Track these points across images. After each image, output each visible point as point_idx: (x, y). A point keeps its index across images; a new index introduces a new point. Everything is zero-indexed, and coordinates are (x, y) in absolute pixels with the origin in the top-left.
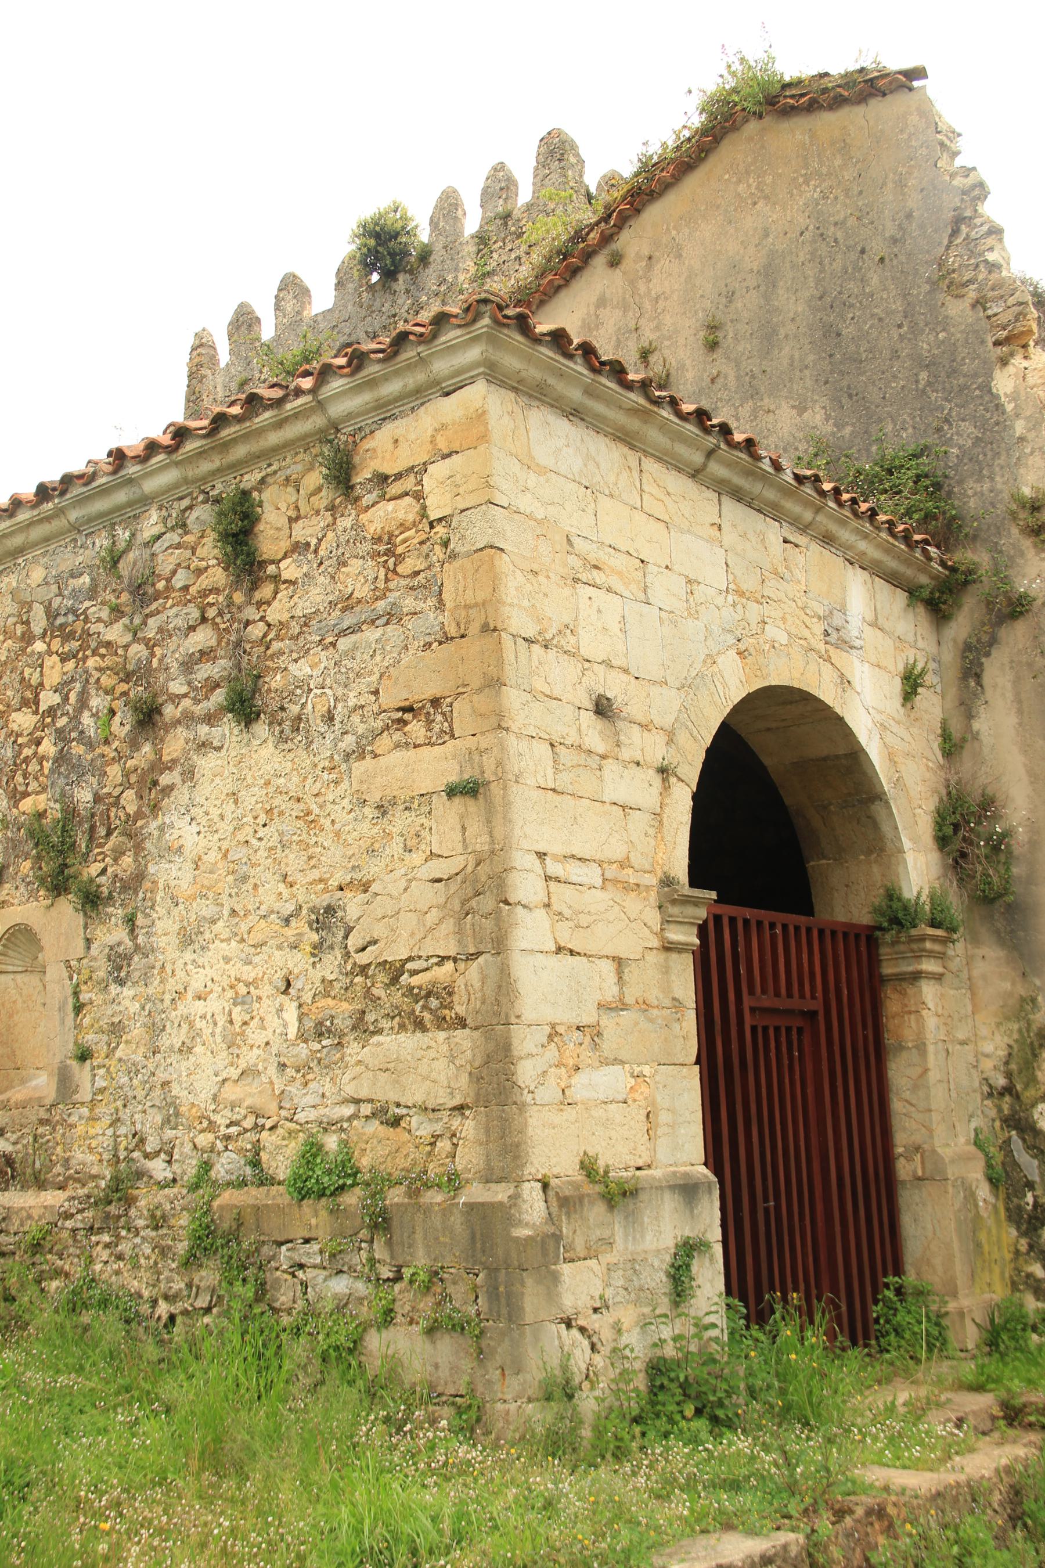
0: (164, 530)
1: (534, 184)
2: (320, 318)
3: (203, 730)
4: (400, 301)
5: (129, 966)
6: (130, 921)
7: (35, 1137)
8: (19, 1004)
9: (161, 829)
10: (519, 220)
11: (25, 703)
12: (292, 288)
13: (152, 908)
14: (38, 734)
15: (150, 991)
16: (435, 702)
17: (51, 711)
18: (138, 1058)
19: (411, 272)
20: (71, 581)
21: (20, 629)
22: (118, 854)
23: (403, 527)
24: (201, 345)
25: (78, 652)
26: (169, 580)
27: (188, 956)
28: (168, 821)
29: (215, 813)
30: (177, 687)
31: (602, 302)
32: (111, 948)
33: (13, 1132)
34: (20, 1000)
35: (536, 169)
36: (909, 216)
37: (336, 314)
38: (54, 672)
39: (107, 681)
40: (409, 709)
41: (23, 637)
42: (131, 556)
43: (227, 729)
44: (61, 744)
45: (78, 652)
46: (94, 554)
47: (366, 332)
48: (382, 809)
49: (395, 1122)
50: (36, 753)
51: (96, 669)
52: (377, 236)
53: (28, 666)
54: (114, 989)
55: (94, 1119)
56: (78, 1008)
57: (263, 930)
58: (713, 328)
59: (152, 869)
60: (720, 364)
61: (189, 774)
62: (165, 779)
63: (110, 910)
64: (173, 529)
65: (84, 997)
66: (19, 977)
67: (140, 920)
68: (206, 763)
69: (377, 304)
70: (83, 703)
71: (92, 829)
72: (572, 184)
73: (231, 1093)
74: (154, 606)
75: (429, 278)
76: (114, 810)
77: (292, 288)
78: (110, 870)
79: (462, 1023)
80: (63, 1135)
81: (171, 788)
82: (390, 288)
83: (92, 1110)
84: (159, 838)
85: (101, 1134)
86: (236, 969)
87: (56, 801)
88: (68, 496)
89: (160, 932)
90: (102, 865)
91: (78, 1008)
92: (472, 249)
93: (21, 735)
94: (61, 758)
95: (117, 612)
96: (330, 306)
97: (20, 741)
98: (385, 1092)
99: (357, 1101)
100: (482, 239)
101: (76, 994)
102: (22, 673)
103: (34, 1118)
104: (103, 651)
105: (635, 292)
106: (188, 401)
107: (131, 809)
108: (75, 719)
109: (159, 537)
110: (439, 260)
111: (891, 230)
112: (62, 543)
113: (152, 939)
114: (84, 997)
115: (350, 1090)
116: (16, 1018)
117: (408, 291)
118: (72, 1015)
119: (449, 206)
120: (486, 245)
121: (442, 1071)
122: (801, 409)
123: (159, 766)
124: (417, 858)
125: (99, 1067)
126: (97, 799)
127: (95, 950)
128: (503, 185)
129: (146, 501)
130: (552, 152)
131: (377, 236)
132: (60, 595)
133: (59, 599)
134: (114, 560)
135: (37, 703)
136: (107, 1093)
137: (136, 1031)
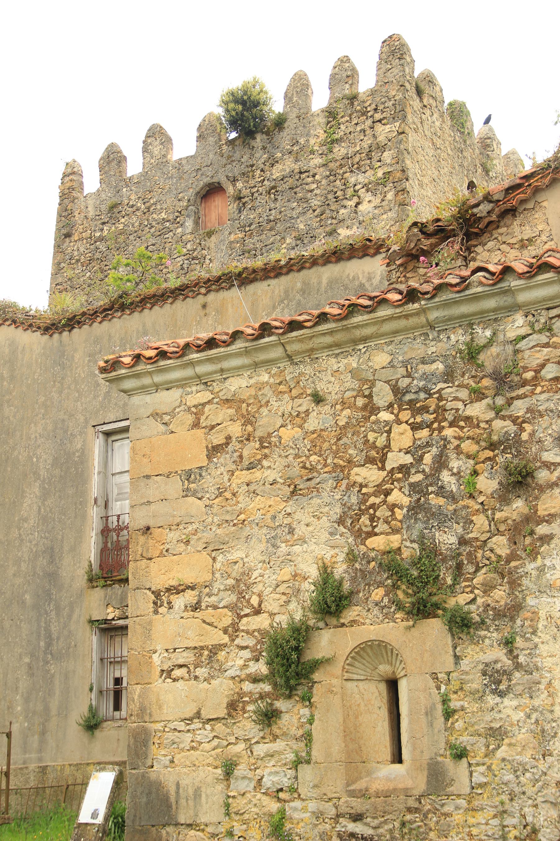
0: (530, 332)
1: (377, 75)
2: (184, 162)
4: (257, 155)
5: (510, 680)
6: (508, 643)
7: (403, 824)
8: (362, 707)
9: (541, 570)
10: (364, 102)
11: (370, 461)
12: (157, 136)
13: (534, 633)
14: (388, 486)
15: (536, 702)
17: (404, 469)
18: (526, 758)
19: (267, 133)
20: (420, 366)
21: (360, 402)
22: (488, 588)
24: (73, 173)
25: (432, 423)
26: (537, 371)
28: (548, 562)
32: (487, 665)
33: (374, 818)
34: (362, 704)
35: (379, 64)
37: (199, 160)
38: (402, 437)
39: (468, 446)
41: (364, 408)
42: (494, 350)
44: (416, 497)
45: (432, 423)
46: (447, 346)
47: (227, 177)
50: (385, 502)
51: (455, 438)
52: (244, 103)
53: (374, 431)
55: (473, 810)
56: (448, 714)
59: (531, 601)
62: (542, 530)
63: (483, 633)
64: (540, 331)
65: (455, 704)
66: (361, 684)
67: (519, 642)
69: (237, 155)
70: (441, 463)
71: (459, 566)
72: (408, 78)
74: (521, 391)
75: (284, 139)
76: (481, 552)
77: (157, 136)
78: (480, 601)
80: (437, 822)
82: (248, 144)
83: (469, 802)
84: (538, 577)
87: (412, 541)
88: (437, 299)
89: (545, 654)
90: (472, 596)
92: (322, 120)
93: (366, 486)
94: (415, 509)
95: (478, 395)
96: (193, 154)
97: (364, 490)
100: (331, 114)
101: (445, 701)
102: (366, 436)
103: (401, 806)
104: (462, 424)
106: (60, 215)
107: (504, 552)
108: (433, 476)
109: (524, 337)
110: (292, 126)
112: (411, 335)
113: (534, 659)
114: (455, 704)
116: (360, 718)
117: (264, 148)
118: (443, 719)
119: (300, 87)
120: (334, 118)
123: (531, 519)
125: (478, 765)
126: (462, 542)
127: (465, 664)
128: (349, 73)
129: (514, 308)
130: (393, 53)
131: (244, 103)
132: (409, 376)
133: (407, 381)
134: (472, 354)
135: (383, 460)
136: (489, 788)
137: (521, 736)
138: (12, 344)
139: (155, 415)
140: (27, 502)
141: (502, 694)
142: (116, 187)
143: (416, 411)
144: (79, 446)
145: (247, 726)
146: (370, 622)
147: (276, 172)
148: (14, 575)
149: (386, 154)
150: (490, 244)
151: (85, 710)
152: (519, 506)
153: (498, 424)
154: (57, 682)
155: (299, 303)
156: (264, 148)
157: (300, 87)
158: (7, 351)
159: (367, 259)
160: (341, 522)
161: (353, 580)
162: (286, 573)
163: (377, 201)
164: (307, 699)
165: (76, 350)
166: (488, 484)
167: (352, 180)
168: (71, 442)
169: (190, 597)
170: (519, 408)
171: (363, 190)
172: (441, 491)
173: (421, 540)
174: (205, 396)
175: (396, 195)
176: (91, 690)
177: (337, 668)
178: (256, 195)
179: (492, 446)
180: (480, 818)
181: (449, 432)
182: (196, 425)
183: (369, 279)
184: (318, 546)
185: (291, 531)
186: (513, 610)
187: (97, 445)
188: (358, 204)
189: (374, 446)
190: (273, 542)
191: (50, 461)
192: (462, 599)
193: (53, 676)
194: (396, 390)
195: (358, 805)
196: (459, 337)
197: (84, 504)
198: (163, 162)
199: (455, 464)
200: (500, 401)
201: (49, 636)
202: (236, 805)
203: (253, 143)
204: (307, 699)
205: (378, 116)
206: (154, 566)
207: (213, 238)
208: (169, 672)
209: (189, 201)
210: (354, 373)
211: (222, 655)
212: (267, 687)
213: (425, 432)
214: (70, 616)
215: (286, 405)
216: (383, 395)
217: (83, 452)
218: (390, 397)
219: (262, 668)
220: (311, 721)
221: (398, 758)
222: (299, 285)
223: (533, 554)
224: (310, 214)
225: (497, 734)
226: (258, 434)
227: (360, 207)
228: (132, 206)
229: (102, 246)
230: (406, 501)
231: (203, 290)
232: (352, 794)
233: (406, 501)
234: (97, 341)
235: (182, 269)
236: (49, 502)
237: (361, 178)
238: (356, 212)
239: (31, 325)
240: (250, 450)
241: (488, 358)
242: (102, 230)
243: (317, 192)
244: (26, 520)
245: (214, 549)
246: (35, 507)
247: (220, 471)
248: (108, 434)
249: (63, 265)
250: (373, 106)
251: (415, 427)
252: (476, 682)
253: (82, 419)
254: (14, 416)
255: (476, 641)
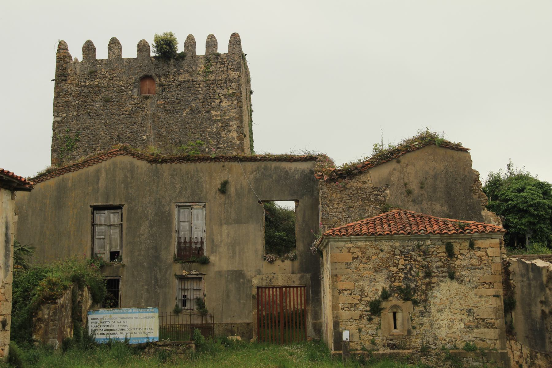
2: (132, 61)
3: (442, 279)
4: (171, 68)
9: (432, 293)
11: (394, 266)
12: (114, 44)
16: (491, 283)
18: (428, 329)
21: (392, 253)
22: (421, 296)
23: (483, 256)
27: (439, 314)
29: (445, 292)
30: (435, 270)
31: (394, 169)
36: (466, 176)
38: (402, 262)
40: (485, 283)
41: (393, 254)
42: (424, 247)
43: (448, 279)
48: (480, 297)
49: (484, 341)
54: (421, 318)
56: (412, 320)
57: (456, 311)
58: (422, 183)
60: (423, 192)
61: (438, 285)
62: (432, 285)
65: (413, 318)
68: (442, 284)
69: (161, 65)
70: (411, 269)
71: (415, 291)
73: (449, 335)
75: (185, 64)
79: (496, 328)
81: (433, 287)
85: (419, 341)
86: (450, 317)
91: (412, 320)
92: (203, 61)
95: (420, 256)
98: (482, 336)
99: (476, 338)
101: (411, 317)
105: (403, 170)
107: (424, 289)
111: (462, 178)
114: (413, 318)
115: (475, 336)
119: (190, 42)
121: (493, 334)
122: (442, 206)
123: (430, 283)
124: (488, 304)
126: (416, 286)
134: (419, 246)
138: (131, 163)
139: (337, 248)
140: (143, 228)
141: (423, 317)
142: (93, 63)
143: (405, 257)
144: (167, 210)
145: (365, 321)
146: (394, 300)
147: (181, 78)
148: (138, 255)
149: (233, 84)
150: (354, 180)
151: (174, 306)
152: (428, 280)
153: (424, 262)
154: (161, 296)
155: (263, 173)
156: (175, 66)
157: (190, 42)
158: (129, 166)
159: (289, 163)
160: (387, 279)
161: (390, 292)
162: (374, 288)
163: (229, 103)
164: (379, 316)
165: (164, 172)
166: (421, 274)
167: (218, 91)
168: (163, 208)
169: (349, 292)
170: (428, 260)
171: (223, 97)
172: (411, 275)
173: (406, 284)
174: (352, 245)
175: (238, 103)
176: (176, 299)
177: (387, 310)
178: (171, 86)
179: (422, 267)
180: (418, 340)
181: (413, 262)
182: (349, 252)
183: (290, 170)
184: (382, 283)
185: (375, 279)
186: (426, 301)
187: (176, 209)
188: (220, 102)
189: (395, 263)
190: (371, 281)
191: (153, 213)
192: (415, 297)
193: (159, 294)
194: (401, 252)
195: (392, 337)
196: (416, 243)
197: (171, 231)
198: (119, 58)
199: (414, 269)
200: (424, 257)
201: (156, 279)
202: (362, 337)
203: (169, 62)
204: (379, 316)
205: (229, 67)
206: (338, 284)
207: (148, 100)
208: (343, 309)
209: (135, 80)
210: (391, 246)
211: (358, 306)
212: (370, 313)
213: (407, 262)
214: (166, 272)
215: (373, 251)
216: (398, 252)
217: (169, 212)
218: (399, 253)
219: (368, 308)
220: (380, 321)
221: (395, 328)
222: (263, 166)
223: (431, 290)
224: (197, 101)
225: (422, 324)
226: (366, 256)
227: (222, 104)
228: (103, 75)
229: (86, 90)
230: (403, 276)
231: (224, 160)
232: (390, 335)
233: (403, 276)
234: (174, 170)
235: (132, 111)
236: (154, 229)
237: (222, 91)
238: (220, 105)
239: (143, 158)
240: (364, 260)
241: (422, 248)
242: (85, 82)
243: (202, 92)
244: (143, 235)
245: (355, 281)
246: (147, 231)
247: (356, 264)
248: (179, 206)
249: (61, 94)
250: (228, 62)
251: (405, 260)
252: (418, 314)
253: (168, 199)
254: (134, 193)
255: (418, 306)
